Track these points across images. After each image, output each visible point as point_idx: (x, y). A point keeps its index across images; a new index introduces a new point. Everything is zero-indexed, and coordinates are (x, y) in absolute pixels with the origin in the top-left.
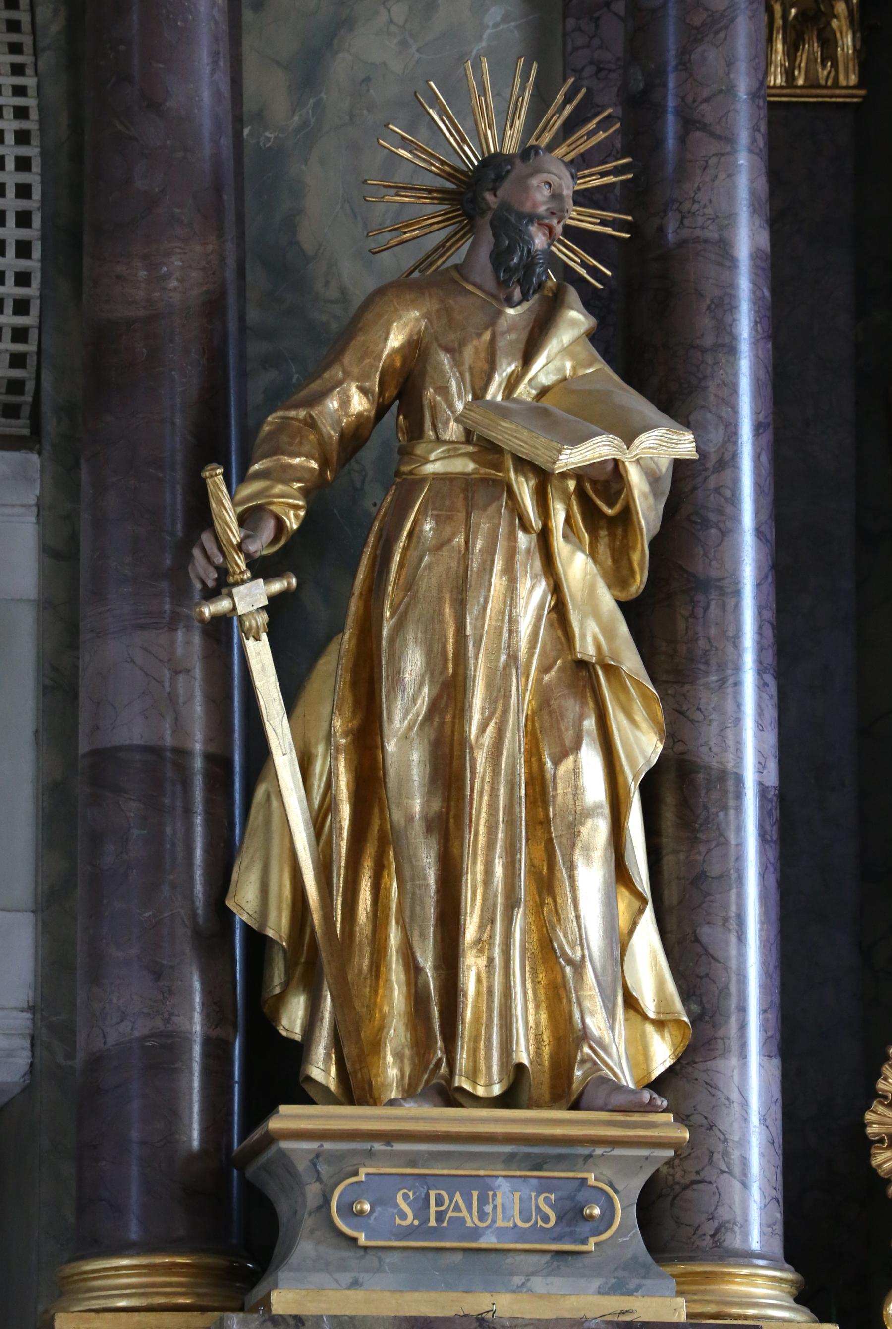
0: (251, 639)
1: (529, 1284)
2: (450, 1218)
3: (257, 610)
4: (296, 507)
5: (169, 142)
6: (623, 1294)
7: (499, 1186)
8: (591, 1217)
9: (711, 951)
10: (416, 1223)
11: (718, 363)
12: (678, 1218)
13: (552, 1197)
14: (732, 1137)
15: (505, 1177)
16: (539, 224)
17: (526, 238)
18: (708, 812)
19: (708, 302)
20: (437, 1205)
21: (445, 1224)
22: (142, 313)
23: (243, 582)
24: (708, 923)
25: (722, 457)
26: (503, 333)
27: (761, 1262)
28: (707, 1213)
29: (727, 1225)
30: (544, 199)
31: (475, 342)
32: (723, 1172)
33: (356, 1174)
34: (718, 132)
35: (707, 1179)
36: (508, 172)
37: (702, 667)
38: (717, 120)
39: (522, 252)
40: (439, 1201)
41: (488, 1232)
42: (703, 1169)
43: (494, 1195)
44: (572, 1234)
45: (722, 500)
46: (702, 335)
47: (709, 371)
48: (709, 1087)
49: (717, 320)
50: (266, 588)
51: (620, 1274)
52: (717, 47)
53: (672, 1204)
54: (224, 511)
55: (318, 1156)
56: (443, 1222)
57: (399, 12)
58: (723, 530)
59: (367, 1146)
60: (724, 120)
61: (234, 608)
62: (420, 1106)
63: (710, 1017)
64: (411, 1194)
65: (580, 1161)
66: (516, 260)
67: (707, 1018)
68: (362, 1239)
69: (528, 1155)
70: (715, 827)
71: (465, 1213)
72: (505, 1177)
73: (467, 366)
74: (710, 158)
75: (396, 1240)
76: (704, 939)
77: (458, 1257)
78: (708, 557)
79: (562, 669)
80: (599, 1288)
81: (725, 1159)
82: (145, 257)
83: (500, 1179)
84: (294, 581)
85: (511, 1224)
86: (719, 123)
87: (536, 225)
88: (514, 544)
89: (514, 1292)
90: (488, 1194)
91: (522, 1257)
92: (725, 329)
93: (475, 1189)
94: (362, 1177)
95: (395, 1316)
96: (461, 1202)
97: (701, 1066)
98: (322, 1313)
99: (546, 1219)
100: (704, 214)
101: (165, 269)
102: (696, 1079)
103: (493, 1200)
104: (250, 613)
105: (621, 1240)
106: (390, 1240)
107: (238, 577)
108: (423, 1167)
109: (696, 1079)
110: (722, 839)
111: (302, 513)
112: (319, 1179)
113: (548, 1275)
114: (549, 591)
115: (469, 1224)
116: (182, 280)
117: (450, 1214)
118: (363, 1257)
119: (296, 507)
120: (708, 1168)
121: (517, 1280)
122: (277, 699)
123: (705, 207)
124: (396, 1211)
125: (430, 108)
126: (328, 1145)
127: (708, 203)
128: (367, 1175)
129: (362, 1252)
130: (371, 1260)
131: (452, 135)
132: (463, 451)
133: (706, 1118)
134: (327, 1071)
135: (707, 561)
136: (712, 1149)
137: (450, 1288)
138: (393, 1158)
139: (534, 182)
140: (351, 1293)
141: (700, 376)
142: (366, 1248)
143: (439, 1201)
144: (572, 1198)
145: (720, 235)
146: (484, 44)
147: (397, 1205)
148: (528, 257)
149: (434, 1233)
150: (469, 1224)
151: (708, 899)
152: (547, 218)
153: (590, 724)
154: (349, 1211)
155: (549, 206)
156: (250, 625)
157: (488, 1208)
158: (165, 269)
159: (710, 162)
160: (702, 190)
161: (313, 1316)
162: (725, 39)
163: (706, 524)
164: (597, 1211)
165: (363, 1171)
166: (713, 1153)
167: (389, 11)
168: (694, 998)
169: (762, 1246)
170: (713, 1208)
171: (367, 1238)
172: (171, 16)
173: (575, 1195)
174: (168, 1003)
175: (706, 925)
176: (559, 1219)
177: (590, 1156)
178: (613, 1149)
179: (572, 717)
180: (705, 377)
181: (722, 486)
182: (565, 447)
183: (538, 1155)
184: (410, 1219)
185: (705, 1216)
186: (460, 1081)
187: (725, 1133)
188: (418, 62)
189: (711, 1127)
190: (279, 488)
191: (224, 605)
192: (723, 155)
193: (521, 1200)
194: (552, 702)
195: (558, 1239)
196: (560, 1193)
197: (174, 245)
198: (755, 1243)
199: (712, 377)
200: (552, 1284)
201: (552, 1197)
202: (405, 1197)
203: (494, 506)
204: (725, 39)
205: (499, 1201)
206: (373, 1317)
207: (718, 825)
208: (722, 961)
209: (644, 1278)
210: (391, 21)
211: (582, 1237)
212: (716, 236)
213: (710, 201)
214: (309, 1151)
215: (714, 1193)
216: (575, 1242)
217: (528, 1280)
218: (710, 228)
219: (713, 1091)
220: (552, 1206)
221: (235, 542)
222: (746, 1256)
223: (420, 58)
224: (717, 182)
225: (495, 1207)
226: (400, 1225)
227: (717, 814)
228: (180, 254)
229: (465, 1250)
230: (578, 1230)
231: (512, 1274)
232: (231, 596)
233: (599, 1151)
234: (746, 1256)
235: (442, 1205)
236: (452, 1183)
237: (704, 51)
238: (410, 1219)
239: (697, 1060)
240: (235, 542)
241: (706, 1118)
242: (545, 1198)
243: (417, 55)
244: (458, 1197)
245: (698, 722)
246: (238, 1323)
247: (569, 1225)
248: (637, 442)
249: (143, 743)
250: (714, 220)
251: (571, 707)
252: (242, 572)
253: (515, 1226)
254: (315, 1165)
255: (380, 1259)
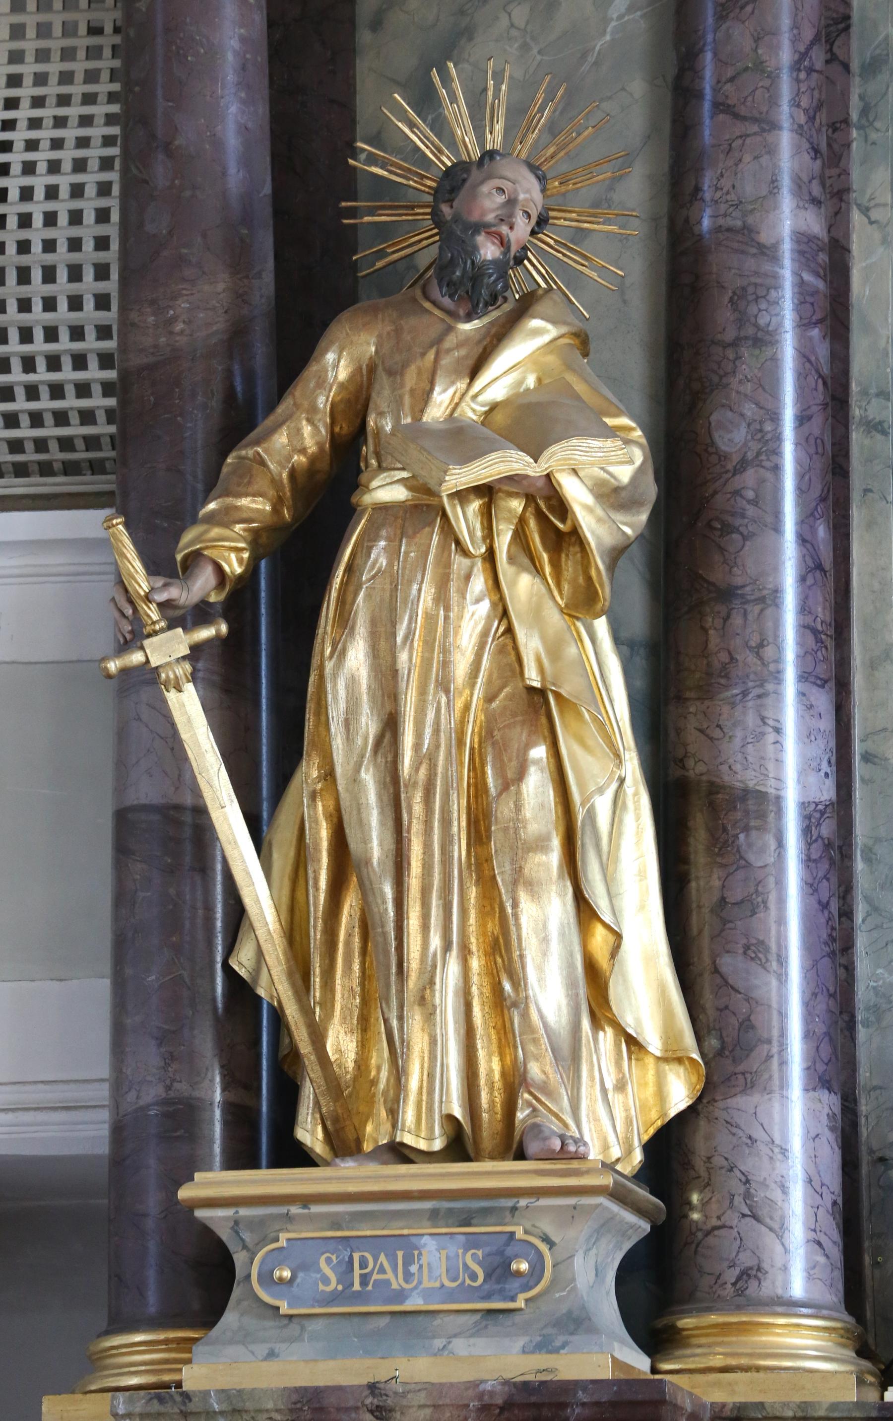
0: (173, 691)
1: (450, 1346)
2: (375, 1280)
3: (178, 660)
4: (238, 550)
5: (176, 182)
6: (550, 1352)
7: (425, 1244)
8: (518, 1273)
9: (730, 981)
10: (340, 1288)
11: (741, 358)
12: (701, 1267)
13: (480, 1253)
14: (754, 1178)
15: (431, 1234)
16: (488, 233)
17: (469, 249)
18: (728, 834)
19: (730, 294)
20: (361, 1268)
21: (370, 1288)
22: (151, 360)
23: (156, 633)
24: (728, 952)
25: (744, 457)
26: (448, 351)
27: (804, 1311)
28: (728, 1260)
29: (749, 1272)
30: (495, 206)
31: (419, 362)
32: (744, 1216)
33: (277, 1240)
34: (743, 113)
35: (727, 1224)
36: (464, 180)
37: (723, 681)
38: (742, 100)
39: (465, 263)
40: (363, 1264)
41: (414, 1294)
42: (724, 1213)
43: (420, 1254)
44: (501, 1291)
45: (744, 502)
46: (724, 330)
47: (729, 367)
48: (729, 1126)
49: (740, 312)
50: (188, 637)
51: (549, 1331)
52: (743, 22)
53: (696, 1252)
54: (126, 562)
55: (236, 1223)
56: (367, 1284)
57: (520, 14)
58: (745, 533)
59: (283, 1210)
60: (750, 99)
61: (148, 661)
62: (360, 1165)
63: (731, 1052)
64: (334, 1257)
65: (508, 1213)
66: (458, 273)
67: (727, 1053)
68: (284, 1308)
69: (450, 1211)
70: (735, 849)
71: (390, 1275)
72: (431, 1234)
73: (408, 388)
74: (734, 141)
75: (320, 1307)
77: (386, 1320)
78: (728, 564)
79: (511, 697)
80: (524, 1347)
81: (748, 1202)
82: (153, 302)
83: (426, 1237)
84: (224, 628)
85: (437, 1284)
86: (744, 103)
87: (483, 233)
88: (447, 571)
89: (435, 1355)
90: (414, 1254)
91: (452, 1317)
92: (749, 320)
93: (400, 1250)
94: (283, 1243)
95: (285, 1388)
96: (386, 1265)
97: (721, 1104)
98: (207, 1388)
99: (474, 1277)
100: (727, 201)
101: (172, 312)
102: (717, 1119)
103: (419, 1259)
104: (168, 664)
105: (557, 1295)
106: (313, 1306)
107: (149, 629)
108: (349, 1229)
109: (717, 1119)
110: (742, 862)
111: (246, 555)
112: (245, 1247)
113: (472, 1336)
114: (495, 616)
115: (395, 1286)
116: (188, 322)
117: (375, 1277)
118: (286, 1326)
119: (238, 550)
120: (729, 1212)
121: (439, 1343)
122: (211, 750)
123: (728, 193)
124: (319, 1276)
125: (400, 121)
126: (244, 1212)
127: (731, 189)
128: (288, 1240)
129: (286, 1321)
130: (294, 1328)
131: (427, 147)
132: (399, 477)
133: (726, 1159)
134: (313, 1133)
135: (727, 568)
136: (733, 1192)
137: (368, 1353)
138: (311, 1219)
139: (485, 188)
140: (265, 1364)
141: (721, 372)
142: (290, 1317)
143: (363, 1264)
144: (501, 1253)
145: (744, 222)
146: (608, 37)
147: (319, 1270)
148: (473, 269)
149: (358, 1298)
150: (395, 1286)
151: (728, 926)
152: (494, 226)
153: (539, 752)
154: (267, 1279)
155: (499, 212)
156: (168, 676)
157: (414, 1268)
158: (172, 312)
159: (734, 145)
160: (725, 176)
161: (200, 1392)
162: (753, 12)
163: (728, 529)
164: (524, 1266)
165: (283, 1236)
166: (734, 1196)
167: (510, 15)
168: (713, 1032)
169: (807, 1291)
170: (734, 1254)
171: (290, 1306)
172: (181, 52)
173: (504, 1251)
174: (170, 1069)
175: (727, 955)
176: (488, 1276)
177: (514, 1209)
178: (538, 1200)
179: (516, 746)
180: (726, 374)
181: (743, 488)
182: (451, 467)
183: (461, 1210)
184: (334, 1284)
185: (726, 1264)
186: (402, 1136)
187: (746, 1174)
188: (539, 65)
189: (732, 1168)
190: (216, 532)
191: (137, 658)
192: (748, 136)
193: (448, 1258)
194: (496, 733)
195: (487, 1297)
196: (488, 1249)
197: (181, 287)
198: (798, 1288)
199: (734, 372)
200: (474, 1345)
201: (480, 1253)
202: (328, 1261)
203: (427, 529)
204: (753, 12)
205: (424, 1261)
206: (262, 1389)
207: (738, 848)
208: (742, 991)
209: (572, 1334)
210: (512, 25)
211: (512, 1294)
212: (739, 223)
213: (734, 187)
214: (226, 1219)
215: (735, 1239)
216: (505, 1299)
217: (449, 1343)
218: (733, 215)
220: (480, 1264)
221: (142, 593)
223: (542, 60)
224: (740, 166)
225: (421, 1267)
226: (322, 1291)
227: (736, 836)
228: (187, 295)
229: (393, 1313)
230: (507, 1286)
231: (434, 1337)
232: (142, 648)
233: (523, 1202)
235: (366, 1267)
236: (376, 1243)
237: (728, 29)
238: (334, 1284)
239: (717, 1098)
240: (142, 593)
241: (726, 1159)
242: (472, 1255)
243: (539, 57)
244: (382, 1258)
245: (718, 739)
246: (124, 1402)
247: (498, 1282)
248: (546, 454)
249: (148, 802)
250: (737, 205)
251: (519, 735)
252: (154, 623)
253: (443, 1286)
254: (237, 1233)
255: (303, 1328)
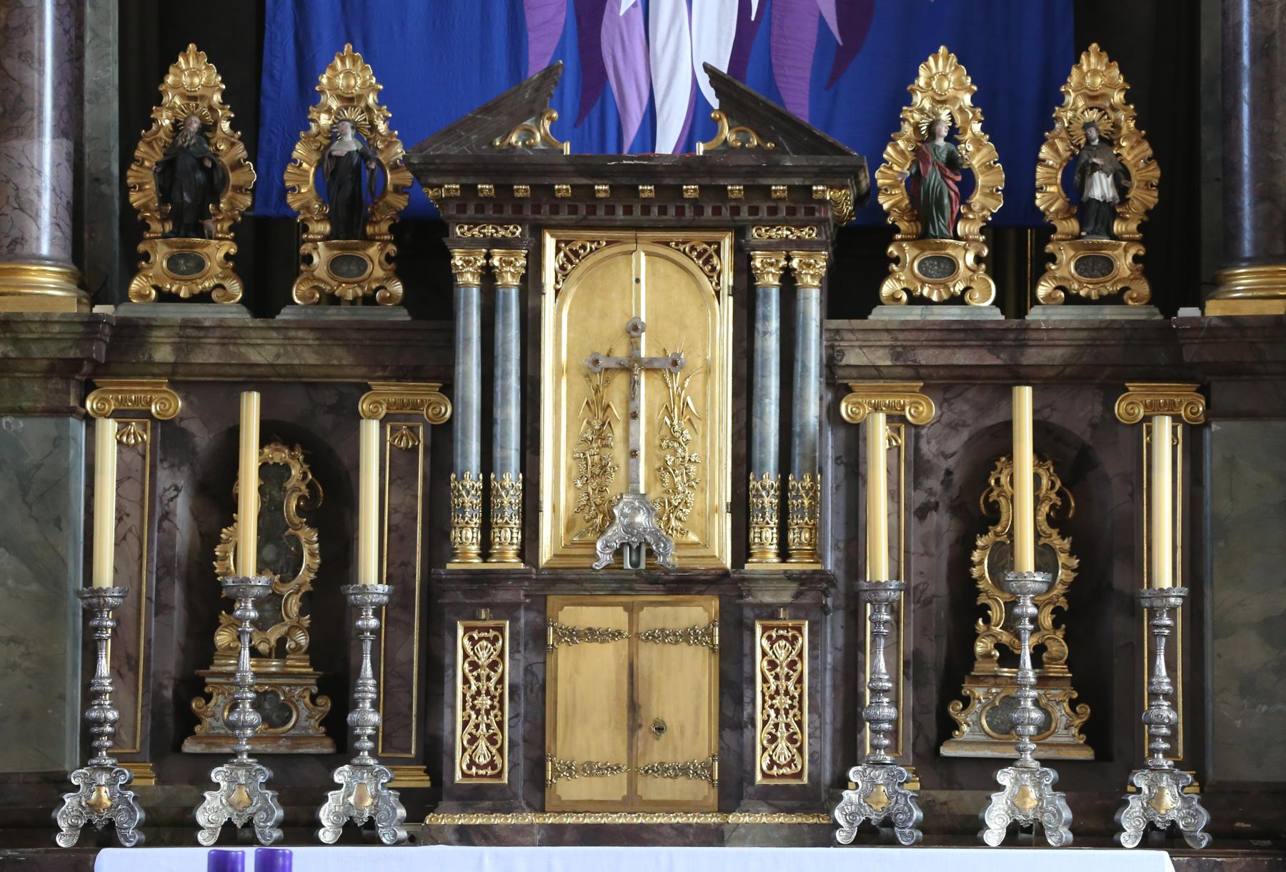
35: (6, 213)
76: (6, 67)
169: (50, 251)
198: (45, 249)
219: (10, 159)
222: (40, 260)
234: (40, 260)
